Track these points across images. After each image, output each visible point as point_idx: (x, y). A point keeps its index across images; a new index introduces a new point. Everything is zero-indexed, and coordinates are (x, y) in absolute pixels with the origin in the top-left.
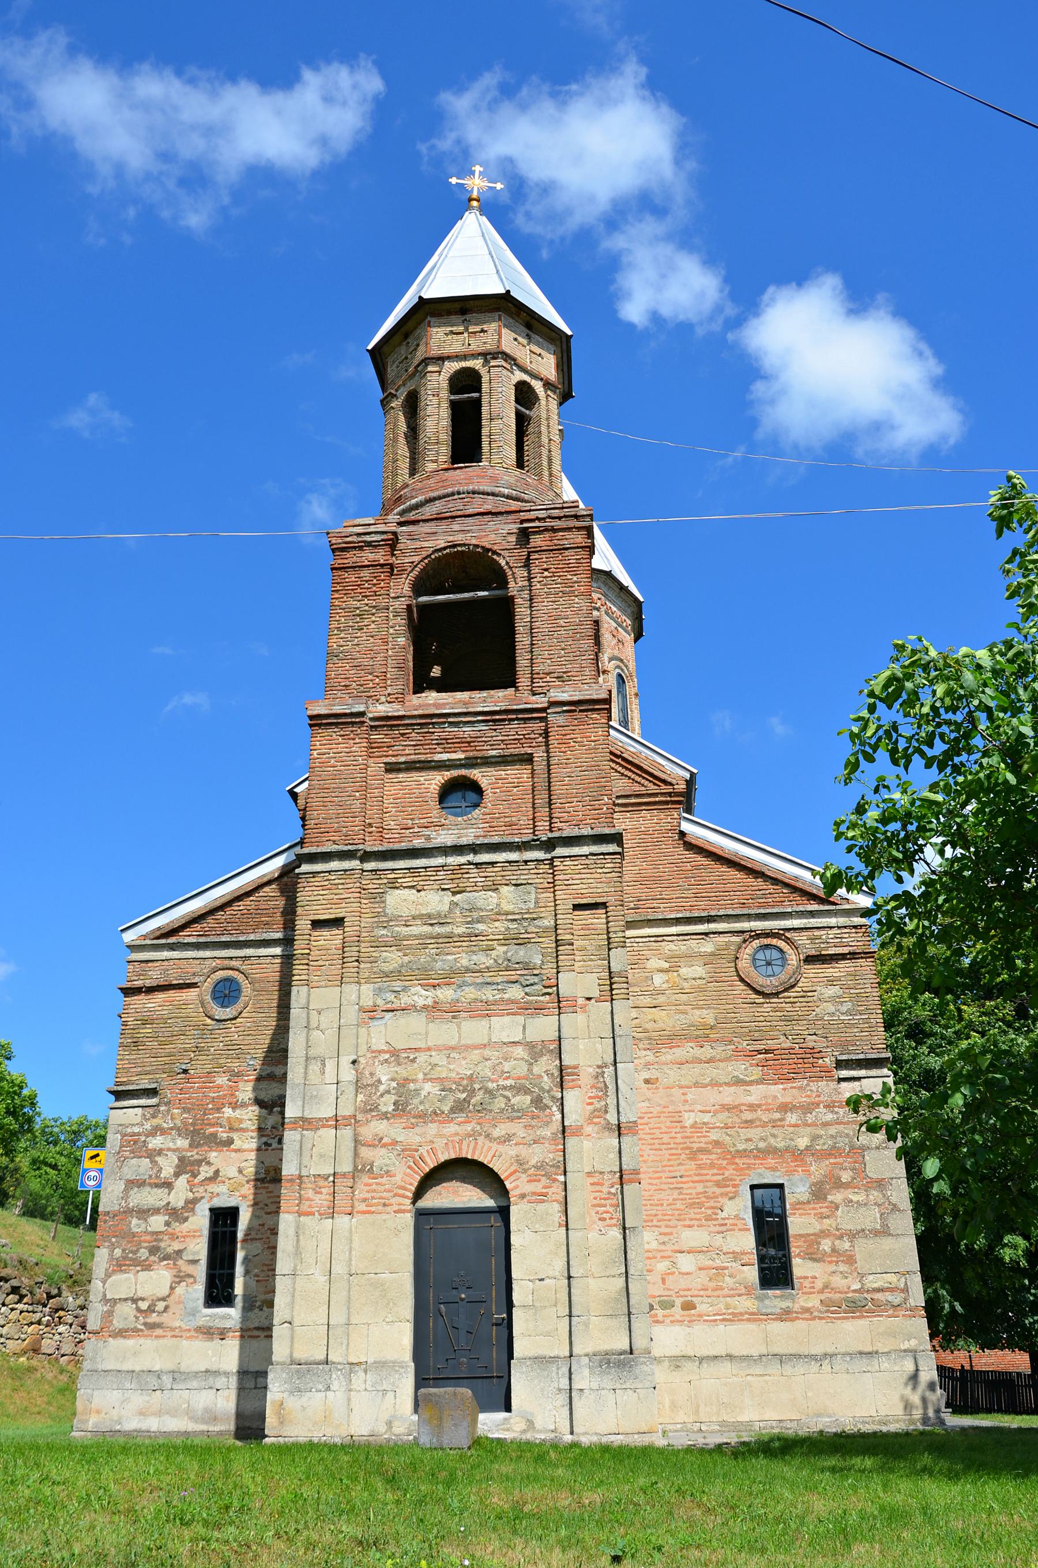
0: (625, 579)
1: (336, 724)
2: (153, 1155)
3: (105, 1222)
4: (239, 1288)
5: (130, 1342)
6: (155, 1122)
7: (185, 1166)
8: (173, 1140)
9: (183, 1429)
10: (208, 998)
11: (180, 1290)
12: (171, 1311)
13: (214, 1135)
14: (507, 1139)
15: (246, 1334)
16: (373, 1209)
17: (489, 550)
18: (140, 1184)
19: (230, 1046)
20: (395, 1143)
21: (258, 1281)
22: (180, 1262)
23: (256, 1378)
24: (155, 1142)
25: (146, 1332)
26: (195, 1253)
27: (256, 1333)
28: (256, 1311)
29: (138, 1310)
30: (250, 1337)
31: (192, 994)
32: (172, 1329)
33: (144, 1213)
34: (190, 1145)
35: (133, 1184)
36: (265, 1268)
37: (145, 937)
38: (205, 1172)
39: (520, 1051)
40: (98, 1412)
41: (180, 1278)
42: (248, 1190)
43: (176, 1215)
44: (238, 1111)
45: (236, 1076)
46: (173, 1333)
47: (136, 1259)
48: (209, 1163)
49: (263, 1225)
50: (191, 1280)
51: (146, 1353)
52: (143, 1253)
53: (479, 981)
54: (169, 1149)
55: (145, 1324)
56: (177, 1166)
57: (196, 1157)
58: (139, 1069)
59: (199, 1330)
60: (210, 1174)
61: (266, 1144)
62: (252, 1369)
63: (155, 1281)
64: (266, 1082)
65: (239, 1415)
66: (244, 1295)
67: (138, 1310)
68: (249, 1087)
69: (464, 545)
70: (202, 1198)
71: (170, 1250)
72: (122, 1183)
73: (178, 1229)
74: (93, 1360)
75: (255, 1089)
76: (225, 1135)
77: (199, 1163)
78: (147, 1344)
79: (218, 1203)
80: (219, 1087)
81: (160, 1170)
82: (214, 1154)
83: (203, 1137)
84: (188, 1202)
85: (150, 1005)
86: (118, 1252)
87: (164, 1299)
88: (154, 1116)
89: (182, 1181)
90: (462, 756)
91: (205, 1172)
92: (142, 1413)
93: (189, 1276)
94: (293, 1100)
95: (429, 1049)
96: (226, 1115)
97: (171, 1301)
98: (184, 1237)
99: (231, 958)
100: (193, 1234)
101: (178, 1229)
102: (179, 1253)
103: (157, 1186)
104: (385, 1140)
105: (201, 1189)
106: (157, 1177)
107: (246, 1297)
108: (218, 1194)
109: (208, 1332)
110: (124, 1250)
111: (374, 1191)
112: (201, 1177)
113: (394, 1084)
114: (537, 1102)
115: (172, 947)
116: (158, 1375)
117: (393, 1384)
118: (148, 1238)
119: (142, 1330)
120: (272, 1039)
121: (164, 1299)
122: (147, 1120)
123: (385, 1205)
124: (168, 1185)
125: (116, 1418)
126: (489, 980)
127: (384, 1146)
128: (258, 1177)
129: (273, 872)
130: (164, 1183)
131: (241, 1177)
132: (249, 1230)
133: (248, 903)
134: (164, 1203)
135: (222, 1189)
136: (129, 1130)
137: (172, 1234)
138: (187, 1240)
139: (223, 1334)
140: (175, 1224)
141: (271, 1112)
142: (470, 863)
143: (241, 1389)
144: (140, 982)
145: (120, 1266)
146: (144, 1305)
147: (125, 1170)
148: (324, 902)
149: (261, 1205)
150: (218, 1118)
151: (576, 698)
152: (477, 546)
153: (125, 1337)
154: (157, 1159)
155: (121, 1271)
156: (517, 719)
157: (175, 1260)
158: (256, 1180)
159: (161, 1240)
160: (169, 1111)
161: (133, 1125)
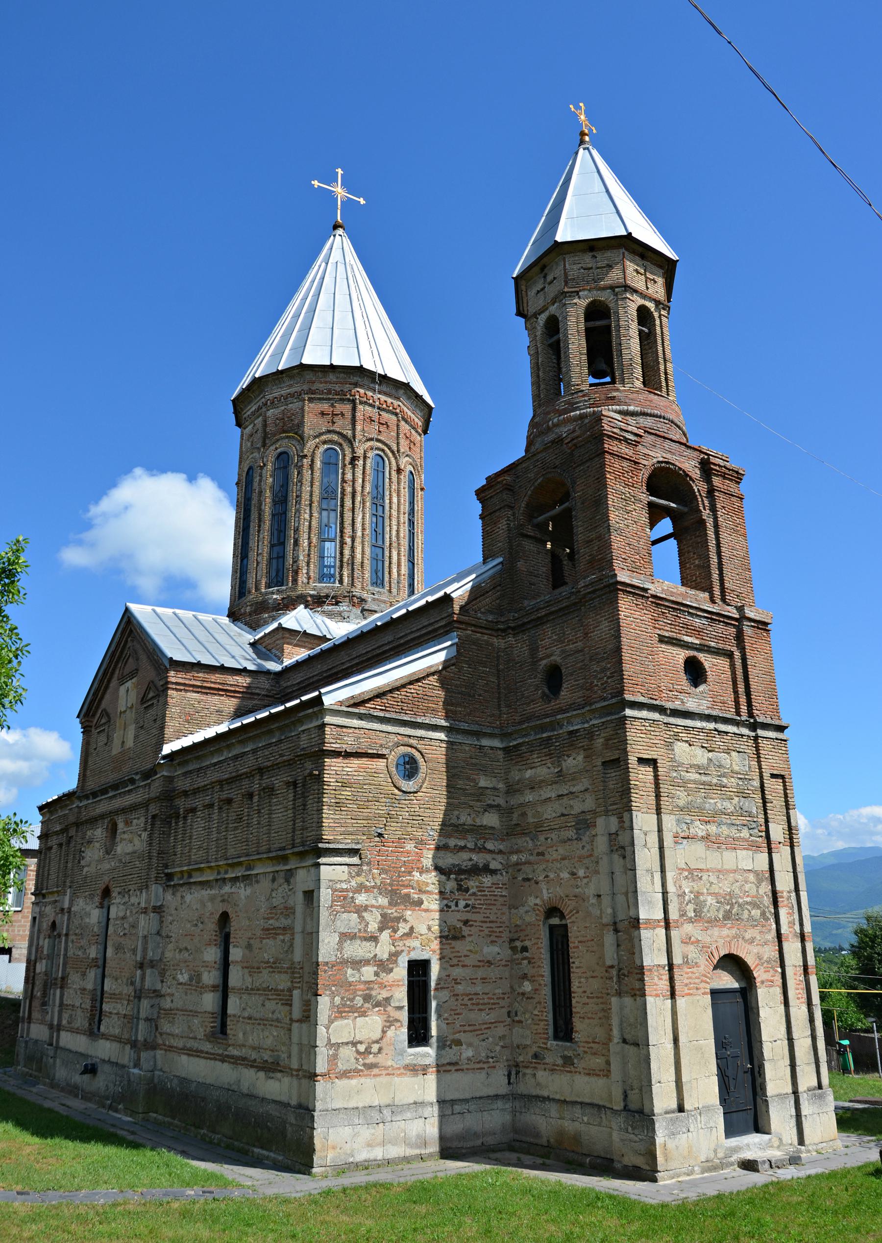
0: (420, 388)
1: (634, 594)
2: (360, 910)
3: (325, 971)
4: (434, 1032)
5: (354, 1082)
6: (360, 879)
7: (388, 923)
8: (375, 898)
9: (402, 1155)
10: (393, 770)
11: (390, 1033)
12: (384, 1052)
13: (408, 895)
14: (752, 941)
15: (441, 1069)
16: (691, 992)
17: (688, 475)
18: (353, 937)
19: (413, 816)
20: (698, 941)
21: (447, 1024)
22: (389, 1009)
23: (452, 1106)
24: (360, 898)
25: (366, 1072)
26: (399, 1000)
27: (448, 1068)
28: (447, 1049)
29: (358, 1052)
30: (444, 1071)
31: (381, 763)
32: (386, 1068)
33: (358, 964)
34: (390, 904)
35: (346, 937)
36: (453, 1013)
37: (341, 703)
38: (403, 928)
39: (751, 877)
40: (334, 1148)
41: (390, 1022)
42: (435, 945)
43: (384, 966)
44: (424, 875)
45: (420, 843)
46: (387, 1072)
47: (353, 1006)
48: (405, 921)
49: (449, 976)
50: (398, 1024)
51: (365, 1091)
52: (359, 1001)
53: (729, 822)
54: (373, 906)
55: (364, 1065)
56: (381, 922)
57: (395, 914)
58: (343, 829)
59: (406, 1067)
60: (407, 930)
61: (447, 906)
62: (447, 1099)
63: (369, 1026)
64: (443, 852)
65: (442, 1138)
66: (438, 1037)
67: (358, 1052)
68: (430, 854)
69: (673, 464)
70: (402, 951)
71: (380, 998)
72: (337, 935)
73: (385, 979)
74: (324, 1100)
75: (434, 857)
76: (416, 896)
77: (398, 919)
78: (367, 1082)
79: (415, 956)
80: (408, 852)
81: (367, 925)
82: (409, 912)
83: (400, 897)
84: (391, 955)
85: (348, 769)
86: (337, 1000)
87: (377, 1042)
88: (358, 875)
89: (385, 936)
90: (697, 642)
91: (403, 928)
92: (370, 1145)
93: (397, 1021)
94: (643, 905)
95: (708, 871)
96: (416, 878)
97: (384, 1043)
98: (390, 986)
99: (410, 736)
100: (396, 984)
101: (385, 979)
102: (388, 1000)
103: (366, 939)
104: (693, 939)
105: (401, 943)
106: (366, 931)
107: (439, 1038)
108: (414, 948)
109: (415, 1069)
110: (342, 998)
111: (691, 978)
112: (400, 933)
113: (692, 896)
114: (763, 914)
115: (361, 717)
116: (380, 1109)
117: (715, 1122)
118: (362, 987)
119: (362, 1071)
120: (444, 815)
121: (377, 1042)
122: (353, 877)
123: (697, 989)
124: (374, 939)
125: (349, 1152)
126: (734, 822)
127: (692, 943)
128: (443, 934)
129: (437, 665)
130: (371, 937)
131: (430, 934)
132: (439, 979)
133: (417, 687)
134: (372, 955)
135: (416, 943)
136: (338, 886)
137: (381, 983)
138: (393, 988)
139: (424, 1070)
140: (383, 975)
141: (449, 879)
142: (716, 730)
143: (442, 1117)
144: (338, 746)
145: (341, 1012)
146: (362, 1048)
147: (338, 923)
148: (644, 744)
149: (447, 959)
150: (410, 880)
151: (758, 618)
152: (680, 469)
153: (349, 1078)
154: (365, 914)
155: (342, 1017)
156: (723, 622)
157: (385, 1007)
158: (440, 937)
159: (372, 989)
160: (370, 870)
161: (341, 881)
